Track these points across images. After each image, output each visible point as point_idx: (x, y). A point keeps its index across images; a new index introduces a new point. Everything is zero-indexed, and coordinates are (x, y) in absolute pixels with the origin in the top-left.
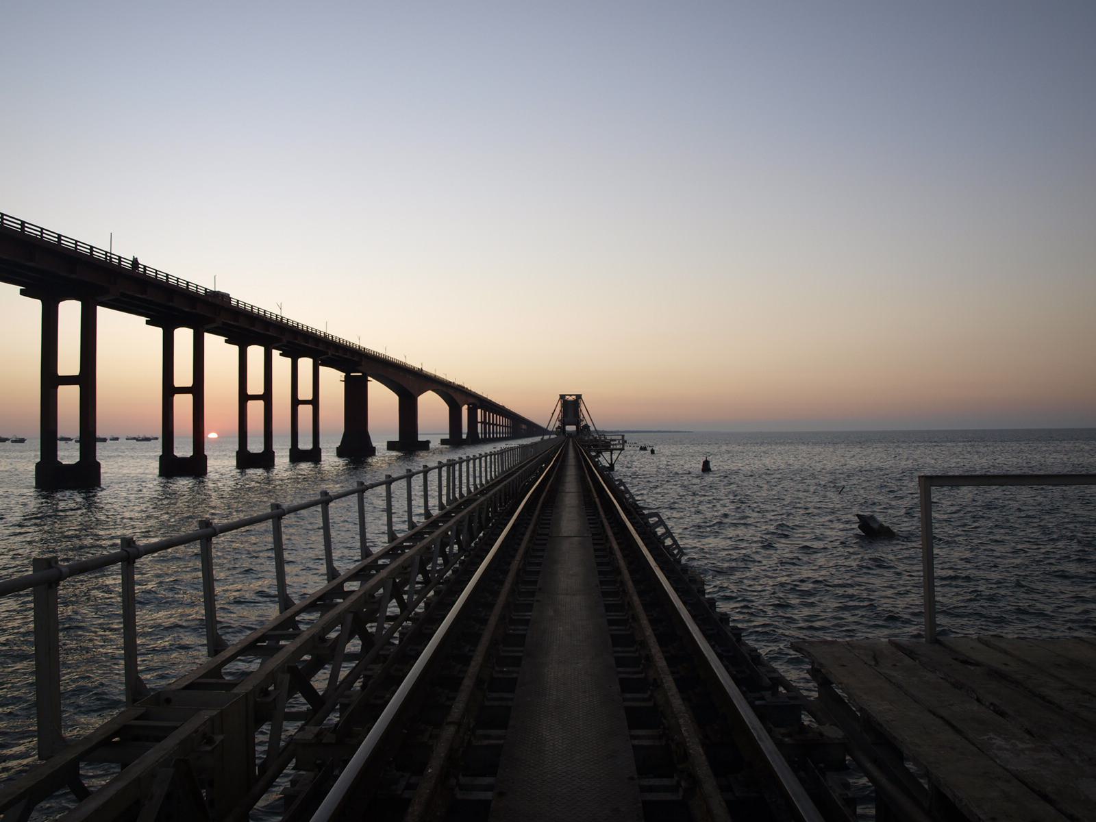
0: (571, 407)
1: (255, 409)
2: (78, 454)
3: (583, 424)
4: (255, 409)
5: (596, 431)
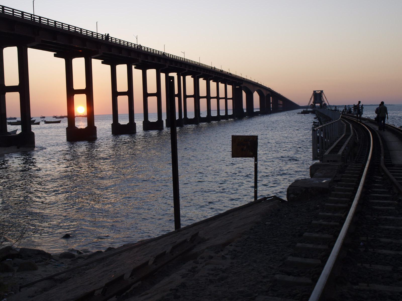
0: (318, 96)
1: (123, 101)
2: (67, 125)
3: (323, 103)
4: (123, 101)
5: (330, 106)
